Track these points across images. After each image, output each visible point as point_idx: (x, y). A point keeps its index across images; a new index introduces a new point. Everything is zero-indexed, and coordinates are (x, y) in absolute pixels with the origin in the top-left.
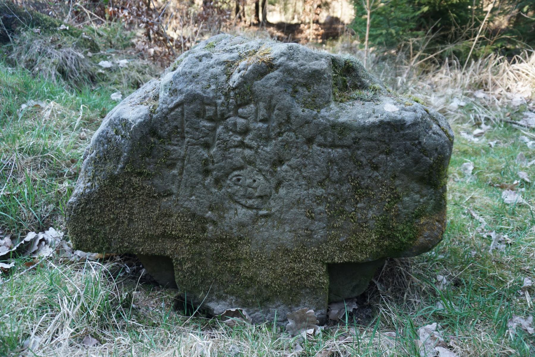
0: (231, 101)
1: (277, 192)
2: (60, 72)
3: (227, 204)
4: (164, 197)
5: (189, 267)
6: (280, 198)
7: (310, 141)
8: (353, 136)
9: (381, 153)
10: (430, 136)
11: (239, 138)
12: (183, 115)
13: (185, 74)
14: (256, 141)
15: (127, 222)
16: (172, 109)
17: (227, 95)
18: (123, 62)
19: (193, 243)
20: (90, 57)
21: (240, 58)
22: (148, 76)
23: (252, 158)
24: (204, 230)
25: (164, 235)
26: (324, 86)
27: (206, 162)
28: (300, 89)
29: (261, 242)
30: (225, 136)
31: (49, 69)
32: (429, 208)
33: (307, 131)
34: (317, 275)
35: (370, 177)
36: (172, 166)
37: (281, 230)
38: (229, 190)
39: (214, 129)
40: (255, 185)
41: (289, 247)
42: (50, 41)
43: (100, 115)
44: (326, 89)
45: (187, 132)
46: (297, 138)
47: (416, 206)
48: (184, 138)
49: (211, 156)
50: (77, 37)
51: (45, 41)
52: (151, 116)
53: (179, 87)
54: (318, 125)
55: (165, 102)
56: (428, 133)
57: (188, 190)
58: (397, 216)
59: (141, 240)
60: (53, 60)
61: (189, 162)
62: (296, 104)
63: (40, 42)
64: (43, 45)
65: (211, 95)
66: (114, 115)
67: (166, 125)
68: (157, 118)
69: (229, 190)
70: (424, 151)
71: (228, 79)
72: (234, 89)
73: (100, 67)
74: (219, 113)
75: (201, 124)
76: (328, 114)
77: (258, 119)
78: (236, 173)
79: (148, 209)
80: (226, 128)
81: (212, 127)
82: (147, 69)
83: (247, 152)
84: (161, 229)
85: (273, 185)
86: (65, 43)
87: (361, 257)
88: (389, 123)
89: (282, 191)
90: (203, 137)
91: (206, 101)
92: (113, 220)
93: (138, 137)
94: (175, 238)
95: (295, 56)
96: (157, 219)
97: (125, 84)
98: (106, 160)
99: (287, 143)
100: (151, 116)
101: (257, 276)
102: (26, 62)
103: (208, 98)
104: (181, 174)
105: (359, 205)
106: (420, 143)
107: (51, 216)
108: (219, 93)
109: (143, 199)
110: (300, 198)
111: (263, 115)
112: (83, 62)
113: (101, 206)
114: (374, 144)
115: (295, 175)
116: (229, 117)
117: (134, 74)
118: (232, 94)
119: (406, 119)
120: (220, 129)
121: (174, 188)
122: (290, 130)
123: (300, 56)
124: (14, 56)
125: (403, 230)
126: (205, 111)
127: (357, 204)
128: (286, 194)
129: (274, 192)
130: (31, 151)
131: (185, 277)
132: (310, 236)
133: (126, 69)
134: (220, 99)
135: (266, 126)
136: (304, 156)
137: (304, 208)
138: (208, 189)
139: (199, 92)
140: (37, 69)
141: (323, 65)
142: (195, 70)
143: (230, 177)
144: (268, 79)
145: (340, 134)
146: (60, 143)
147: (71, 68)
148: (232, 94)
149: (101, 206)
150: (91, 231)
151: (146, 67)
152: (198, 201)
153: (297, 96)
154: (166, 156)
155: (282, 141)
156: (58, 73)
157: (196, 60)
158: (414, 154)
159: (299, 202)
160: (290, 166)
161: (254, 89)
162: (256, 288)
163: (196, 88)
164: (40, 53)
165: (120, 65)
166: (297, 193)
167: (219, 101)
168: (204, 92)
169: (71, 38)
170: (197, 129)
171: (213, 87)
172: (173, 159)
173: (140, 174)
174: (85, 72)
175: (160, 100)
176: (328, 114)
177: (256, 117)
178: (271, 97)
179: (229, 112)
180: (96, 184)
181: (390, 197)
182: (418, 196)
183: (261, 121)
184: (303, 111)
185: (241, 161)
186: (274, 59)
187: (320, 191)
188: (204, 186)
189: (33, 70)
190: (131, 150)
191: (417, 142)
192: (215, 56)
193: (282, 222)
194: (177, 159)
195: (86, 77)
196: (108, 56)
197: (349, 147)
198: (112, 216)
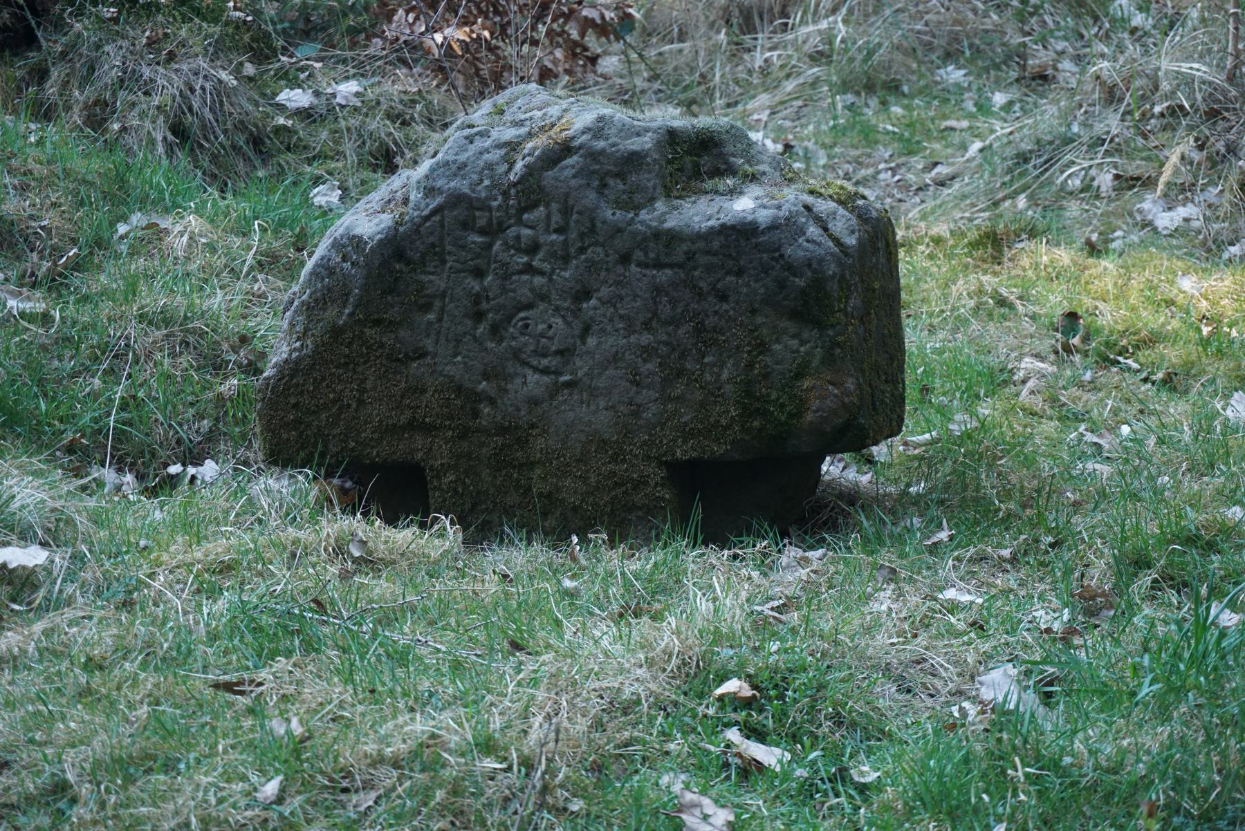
0: (511, 202)
1: (584, 343)
2: (174, 133)
3: (511, 367)
4: (414, 359)
5: (451, 482)
6: (589, 352)
7: (625, 259)
8: (685, 248)
9: (727, 273)
10: (800, 245)
11: (525, 259)
12: (442, 226)
13: (447, 164)
14: (550, 263)
15: (354, 405)
16: (427, 218)
17: (506, 194)
18: (348, 89)
19: (459, 438)
20: (251, 79)
21: (530, 135)
22: (420, 129)
23: (545, 289)
24: (476, 414)
25: (414, 426)
26: (646, 176)
27: (477, 299)
28: (611, 182)
29: (563, 428)
30: (504, 257)
31: (148, 125)
32: (815, 362)
33: (620, 243)
34: (652, 483)
35: (716, 312)
36: (427, 308)
37: (593, 408)
38: (513, 343)
39: (490, 246)
40: (551, 333)
41: (606, 436)
42: (144, 41)
43: (294, 244)
44: (649, 180)
45: (449, 253)
46: (607, 255)
47: (795, 359)
48: (444, 262)
49: (484, 289)
50: (216, 21)
51: (133, 45)
52: (396, 230)
53: (439, 184)
54: (634, 234)
55: (417, 208)
56: (796, 241)
57: (451, 345)
58: (766, 376)
59: (376, 436)
60: (156, 100)
61: (452, 300)
62: (603, 204)
63: (121, 47)
64: (128, 55)
65: (483, 195)
66: (341, 231)
67: (418, 243)
68: (405, 232)
69: (513, 343)
70: (790, 268)
71: (510, 169)
72: (515, 185)
73: (281, 108)
74: (495, 221)
75: (469, 239)
76: (649, 217)
77: (551, 229)
78: (522, 315)
79: (389, 380)
80: (505, 243)
81: (485, 243)
82: (418, 107)
83: (538, 280)
84: (408, 414)
85: (577, 332)
86: (183, 44)
87: (719, 449)
88: (733, 227)
89: (592, 341)
90: (472, 260)
91: (476, 204)
92: (334, 401)
93: (377, 263)
94: (428, 429)
95: (606, 131)
96: (402, 397)
97: (352, 158)
98: (325, 303)
99: (594, 263)
100: (396, 230)
101: (558, 489)
102: (86, 107)
103: (478, 199)
104: (440, 320)
105: (706, 360)
106: (782, 256)
107: (209, 440)
108: (495, 192)
109: (381, 364)
110: (617, 352)
111: (557, 223)
112: (234, 99)
113: (315, 379)
114: (715, 260)
115: (608, 314)
116: (509, 227)
117: (377, 124)
118: (513, 191)
119: (760, 220)
120: (497, 246)
121: (429, 344)
122: (596, 244)
123: (613, 131)
124: (51, 89)
125: (778, 399)
126: (474, 219)
127: (703, 357)
128: (597, 345)
129: (578, 342)
130: (165, 319)
131: (445, 500)
132: (636, 414)
133: (356, 109)
134: (496, 200)
135: (562, 238)
136: (618, 283)
137: (626, 368)
138: (481, 344)
139: (466, 190)
140: (116, 126)
141: (645, 142)
142: (462, 158)
143: (514, 321)
144: (563, 169)
145: (667, 246)
146: (217, 301)
147: (202, 119)
148: (513, 191)
149: (315, 379)
150: (298, 422)
151: (414, 102)
152: (465, 363)
153: (606, 192)
154: (417, 291)
155: (586, 260)
156: (170, 137)
157: (465, 142)
158: (774, 273)
159: (616, 358)
160: (599, 299)
161: (544, 183)
162: (558, 514)
163: (461, 185)
164: (122, 81)
165: (339, 100)
166: (613, 342)
167: (495, 204)
168: (473, 191)
169: (200, 28)
170: (463, 247)
171: (487, 182)
172: (428, 296)
173: (378, 322)
174: (241, 126)
175: (411, 205)
176: (649, 217)
177: (549, 226)
178: (567, 195)
179: (509, 219)
180: (309, 342)
181: (749, 344)
182: (796, 342)
183: (556, 231)
184: (614, 214)
185: (529, 294)
186: (573, 138)
187: (646, 338)
188: (475, 339)
189: (106, 130)
190: (366, 284)
191: (777, 255)
192: (494, 134)
193: (594, 393)
194: (434, 296)
195: (241, 140)
196: (302, 70)
197: (680, 266)
198: (331, 396)
